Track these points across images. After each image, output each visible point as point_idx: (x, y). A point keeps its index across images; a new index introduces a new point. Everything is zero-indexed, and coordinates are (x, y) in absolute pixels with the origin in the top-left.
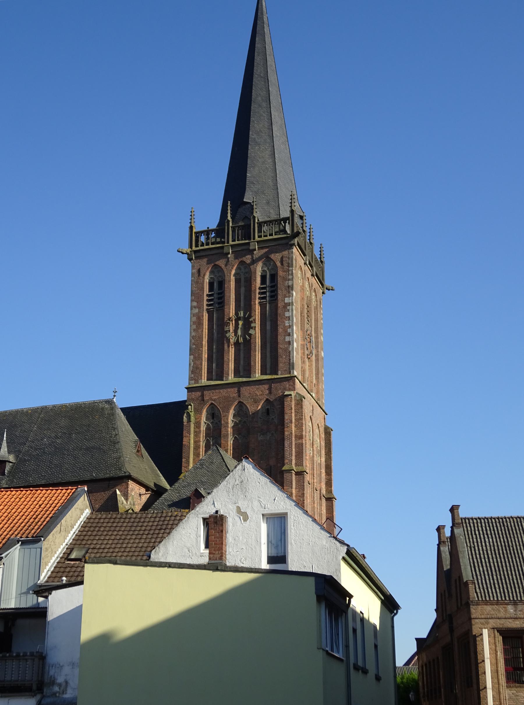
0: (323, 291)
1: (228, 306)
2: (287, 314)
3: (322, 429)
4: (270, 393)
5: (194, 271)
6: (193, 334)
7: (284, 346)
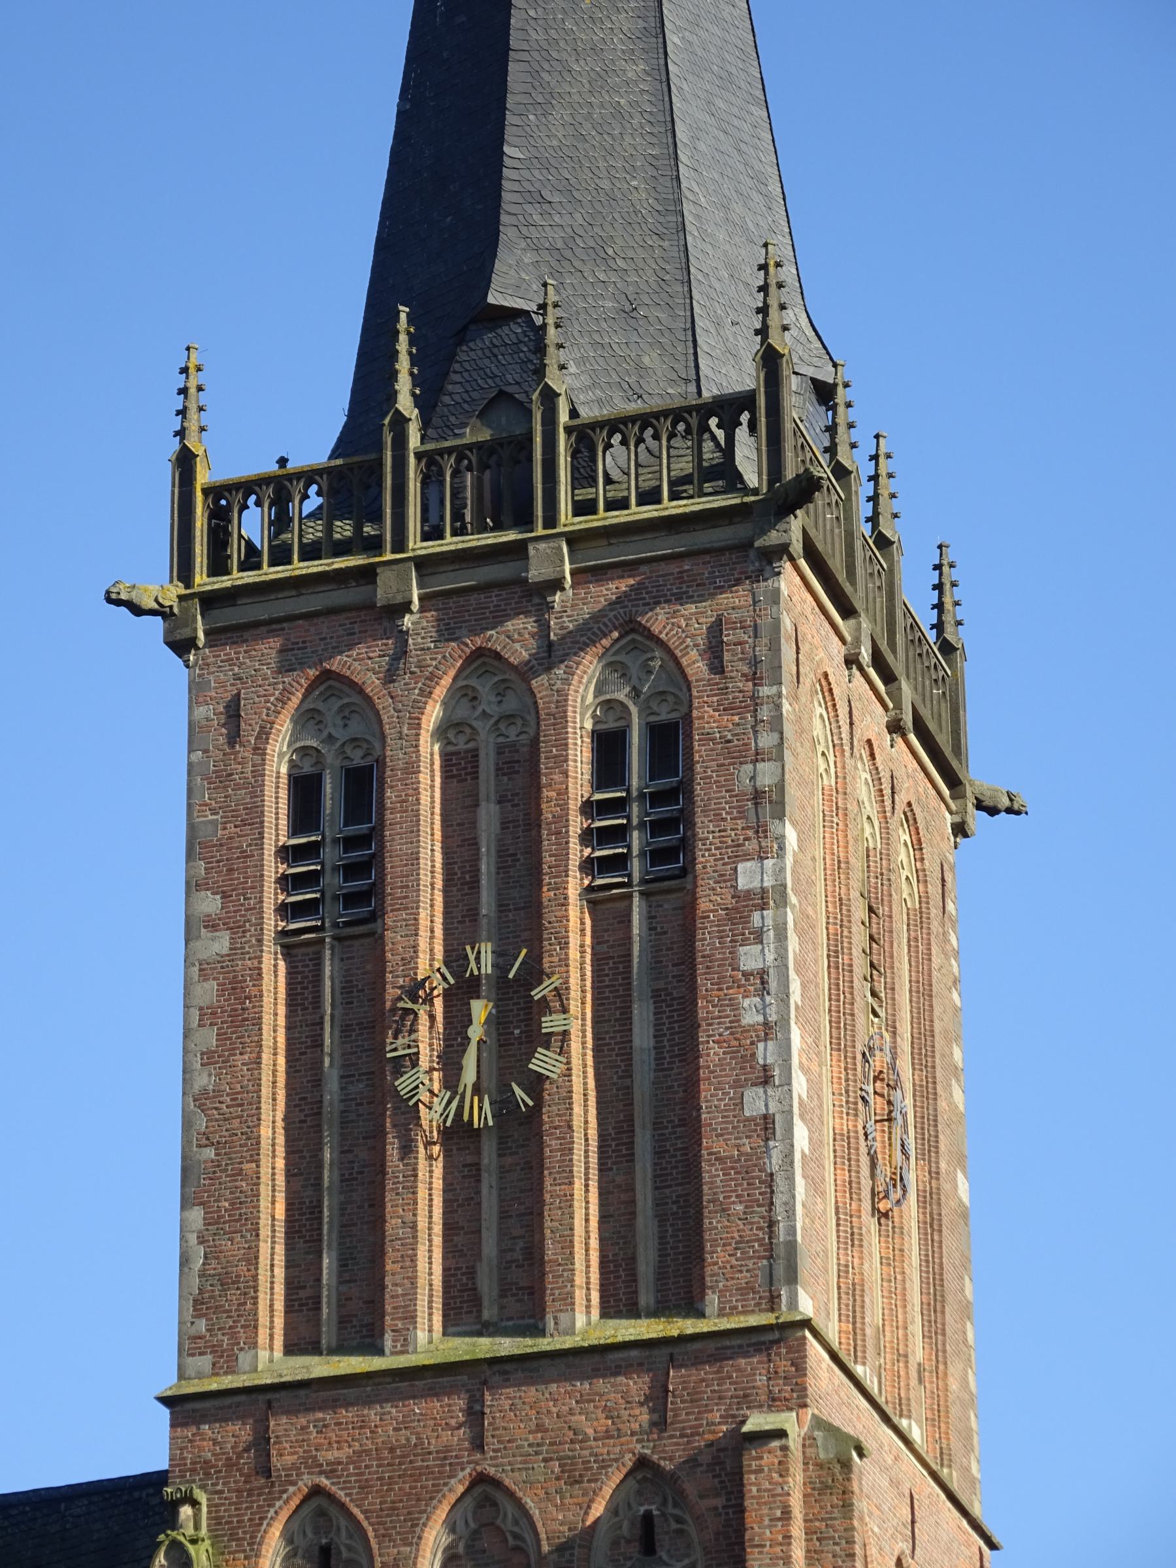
0: (957, 819)
2: (750, 958)
4: (660, 1423)
5: (201, 712)
6: (203, 1080)
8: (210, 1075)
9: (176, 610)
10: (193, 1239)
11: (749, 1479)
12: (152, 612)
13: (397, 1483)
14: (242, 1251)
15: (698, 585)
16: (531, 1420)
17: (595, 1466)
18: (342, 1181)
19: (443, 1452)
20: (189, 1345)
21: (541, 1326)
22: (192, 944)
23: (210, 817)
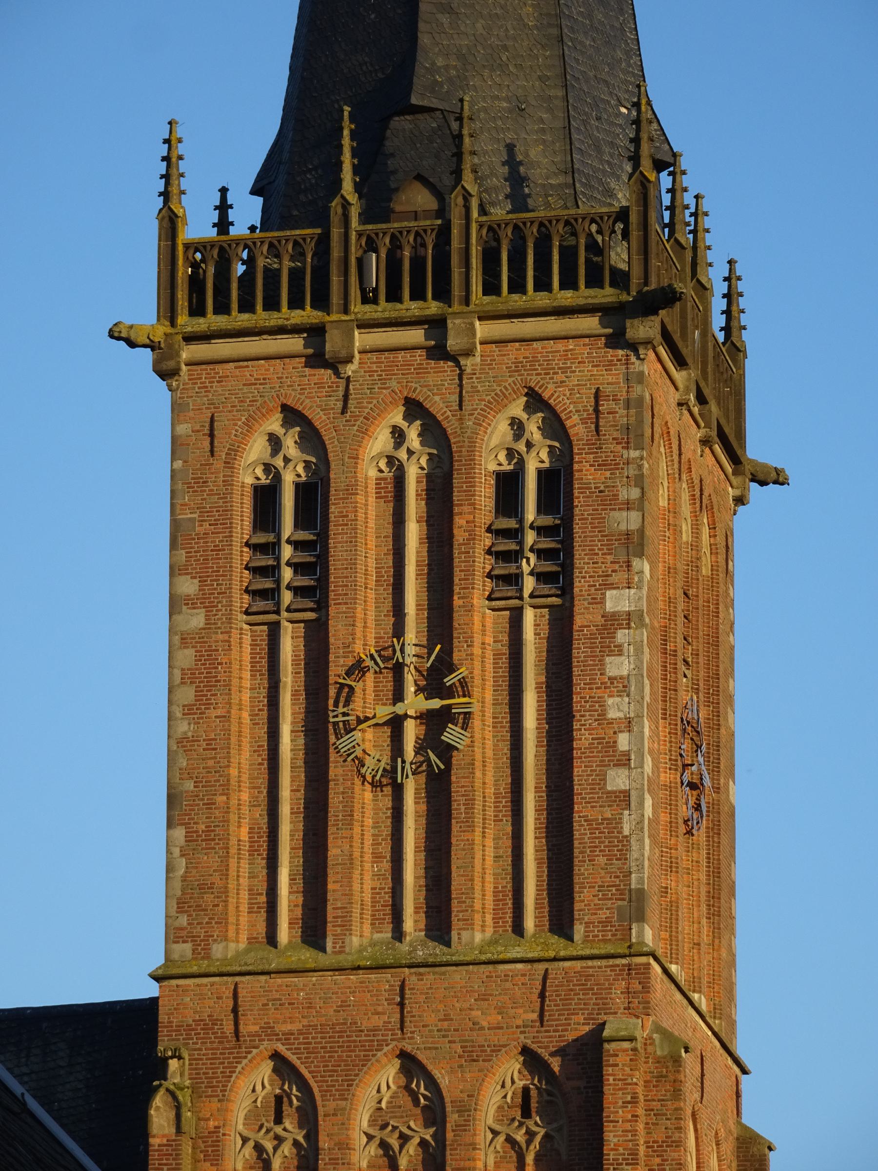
0: (738, 493)
1: (343, 608)
3: (728, 1147)
5: (183, 429)
6: (183, 727)
7: (602, 813)
8: (189, 724)
9: (162, 345)
10: (176, 851)
11: (607, 1070)
12: (145, 346)
13: (336, 1052)
14: (217, 864)
15: (579, 363)
16: (439, 1011)
17: (489, 1049)
18: (291, 813)
19: (372, 1030)
20: (173, 935)
21: (446, 939)
22: (174, 617)
23: (190, 516)
